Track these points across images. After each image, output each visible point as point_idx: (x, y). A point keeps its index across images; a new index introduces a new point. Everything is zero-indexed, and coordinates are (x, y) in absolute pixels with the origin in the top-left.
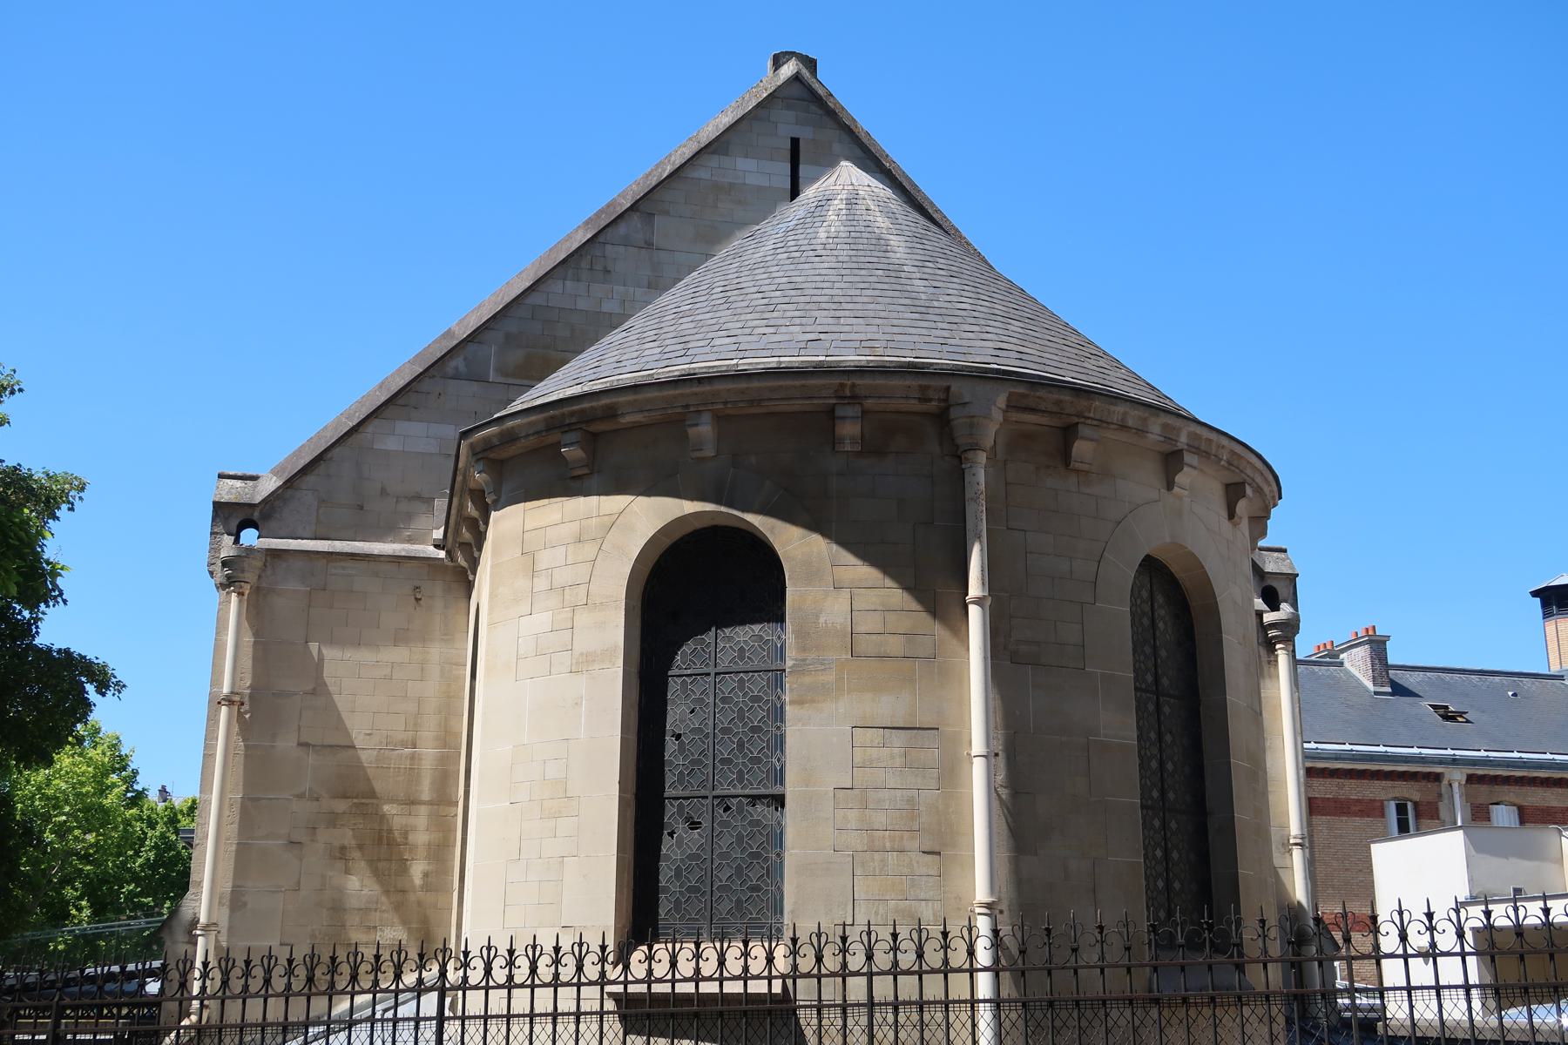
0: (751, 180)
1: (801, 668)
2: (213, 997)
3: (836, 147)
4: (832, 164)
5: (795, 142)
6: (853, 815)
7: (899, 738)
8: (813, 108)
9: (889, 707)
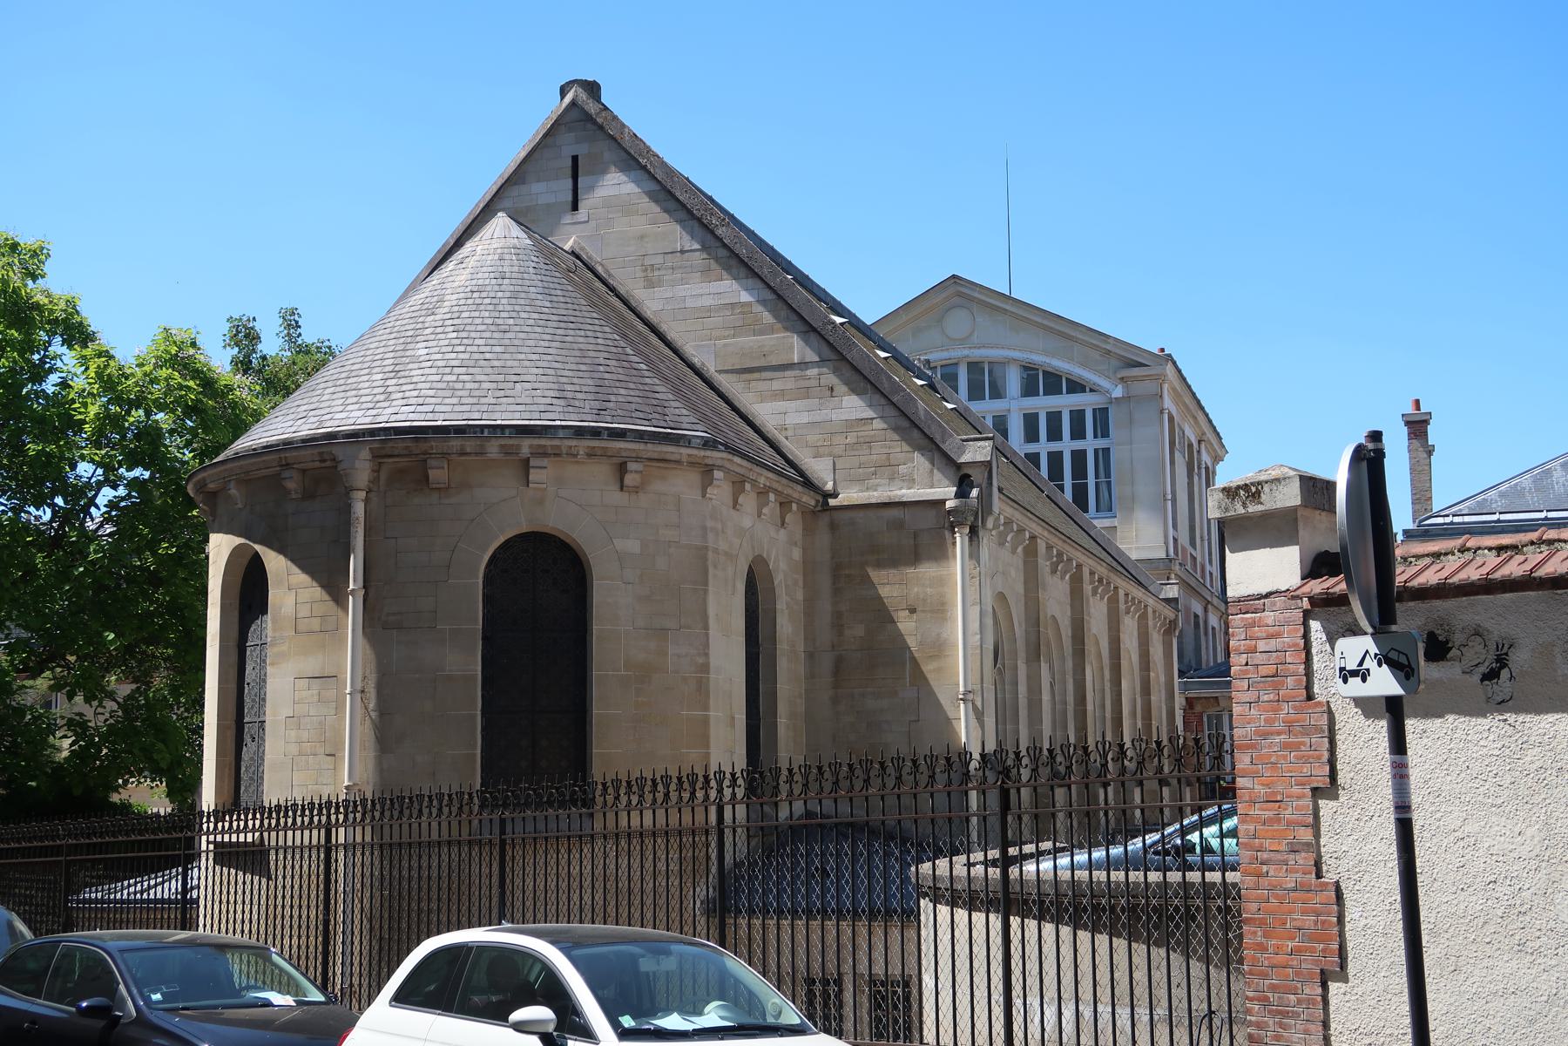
0: (543, 200)
1: (273, 645)
2: (741, 802)
3: (607, 155)
4: (604, 172)
5: (575, 159)
6: (293, 733)
7: (316, 683)
8: (589, 126)
9: (312, 665)
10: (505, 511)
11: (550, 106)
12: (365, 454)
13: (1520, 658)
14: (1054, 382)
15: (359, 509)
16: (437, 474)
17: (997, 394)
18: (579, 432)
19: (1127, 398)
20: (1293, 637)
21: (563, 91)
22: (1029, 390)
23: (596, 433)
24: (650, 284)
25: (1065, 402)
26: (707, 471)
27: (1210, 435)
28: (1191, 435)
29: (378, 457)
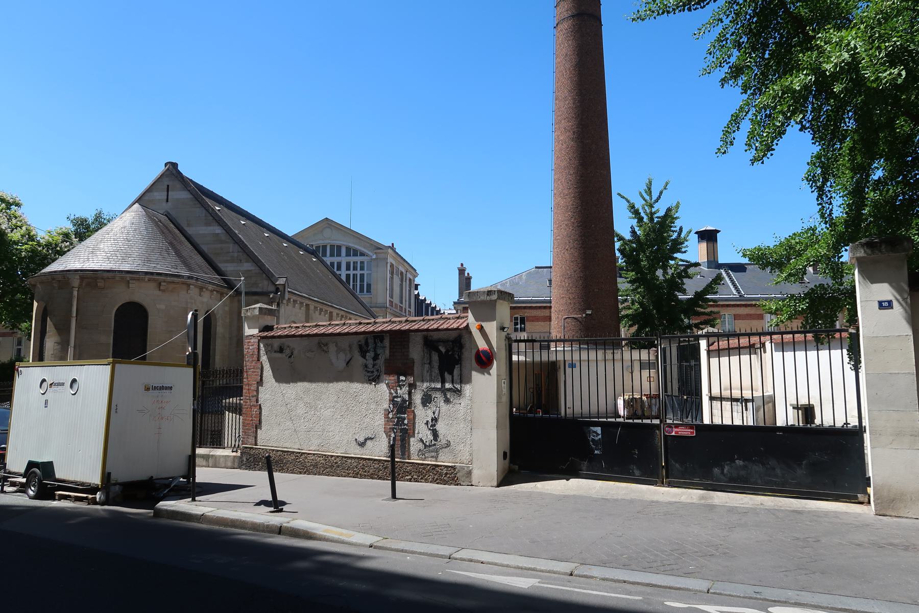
10: (122, 296)
11: (161, 169)
12: (78, 277)
13: (295, 352)
14: (356, 253)
15: (75, 293)
16: (101, 284)
17: (339, 255)
18: (146, 273)
19: (376, 259)
20: (256, 346)
21: (166, 165)
22: (348, 255)
23: (152, 274)
24: (189, 225)
25: (359, 259)
26: (189, 285)
27: (410, 269)
28: (401, 269)
29: (82, 278)
